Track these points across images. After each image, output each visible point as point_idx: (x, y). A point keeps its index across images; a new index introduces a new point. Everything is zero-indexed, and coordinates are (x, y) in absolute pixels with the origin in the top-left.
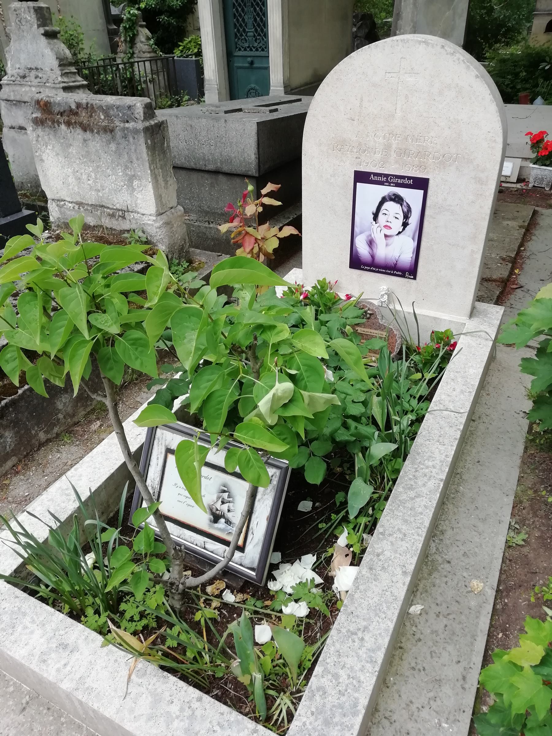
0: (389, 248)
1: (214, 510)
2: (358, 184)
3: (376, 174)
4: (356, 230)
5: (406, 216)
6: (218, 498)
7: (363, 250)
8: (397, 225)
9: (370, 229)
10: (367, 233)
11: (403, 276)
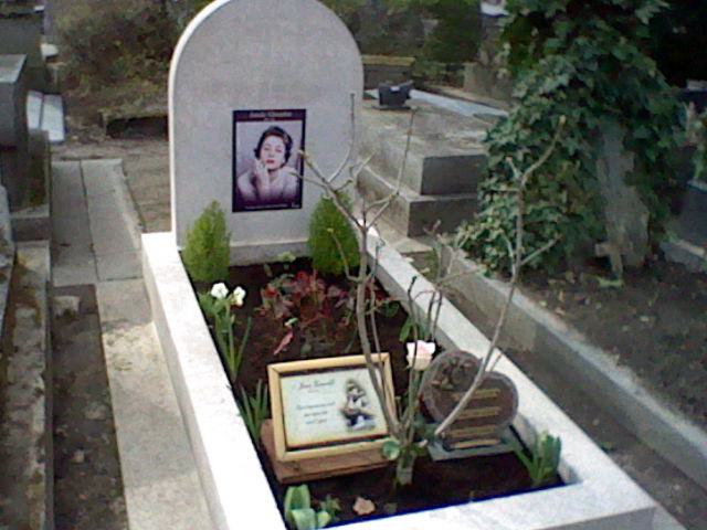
0: (275, 182)
1: (349, 413)
2: (238, 124)
3: (255, 111)
4: (238, 170)
5: (288, 147)
6: (348, 398)
7: (245, 186)
8: (279, 158)
9: (253, 167)
10: (249, 172)
11: (289, 207)
